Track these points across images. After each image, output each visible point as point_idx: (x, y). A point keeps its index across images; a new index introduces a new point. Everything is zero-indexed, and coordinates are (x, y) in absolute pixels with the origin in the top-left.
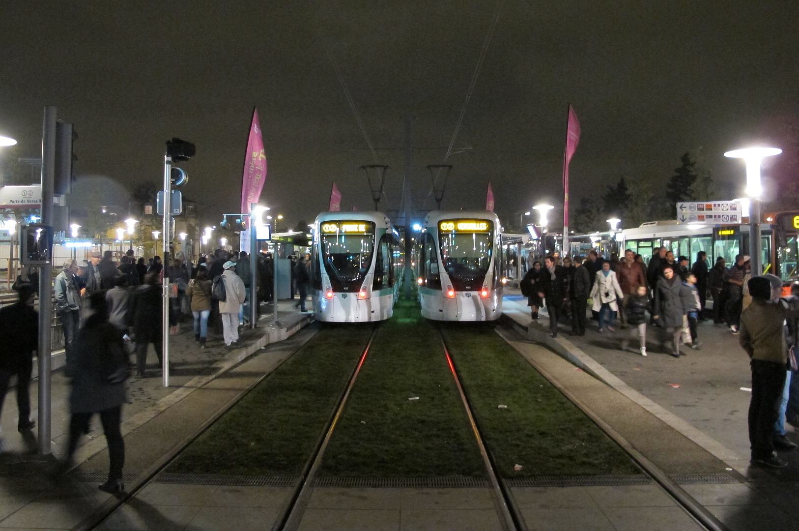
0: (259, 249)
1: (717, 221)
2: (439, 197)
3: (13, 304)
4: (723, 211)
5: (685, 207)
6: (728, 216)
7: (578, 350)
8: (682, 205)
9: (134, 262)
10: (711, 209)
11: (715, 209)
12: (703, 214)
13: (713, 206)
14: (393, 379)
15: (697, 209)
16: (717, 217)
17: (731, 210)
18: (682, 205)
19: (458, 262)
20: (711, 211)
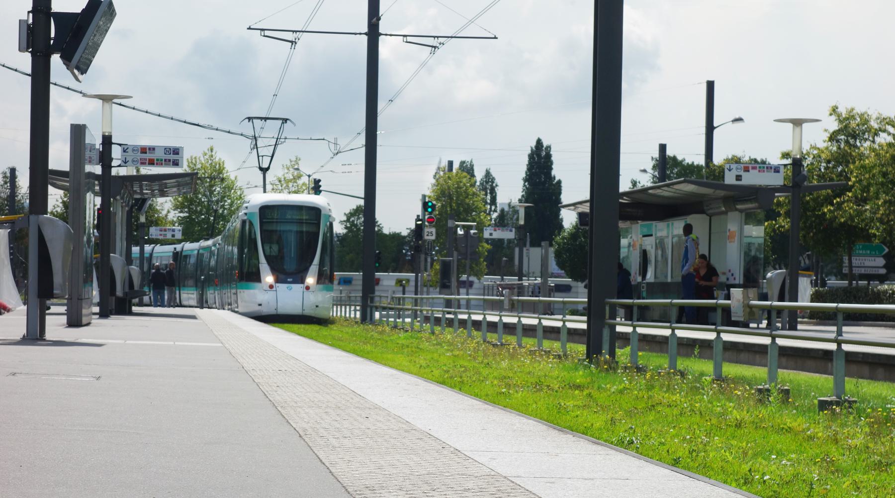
0: (209, 271)
1: (152, 153)
2: (265, 165)
3: (708, 258)
4: (166, 155)
5: (126, 158)
6: (170, 149)
7: (869, 384)
8: (728, 169)
9: (362, 208)
10: (146, 153)
11: (149, 153)
12: (153, 158)
13: (155, 160)
14: (714, 495)
15: (139, 152)
16: (151, 149)
17: (173, 154)
18: (728, 169)
19: (730, 179)
20: (145, 155)
